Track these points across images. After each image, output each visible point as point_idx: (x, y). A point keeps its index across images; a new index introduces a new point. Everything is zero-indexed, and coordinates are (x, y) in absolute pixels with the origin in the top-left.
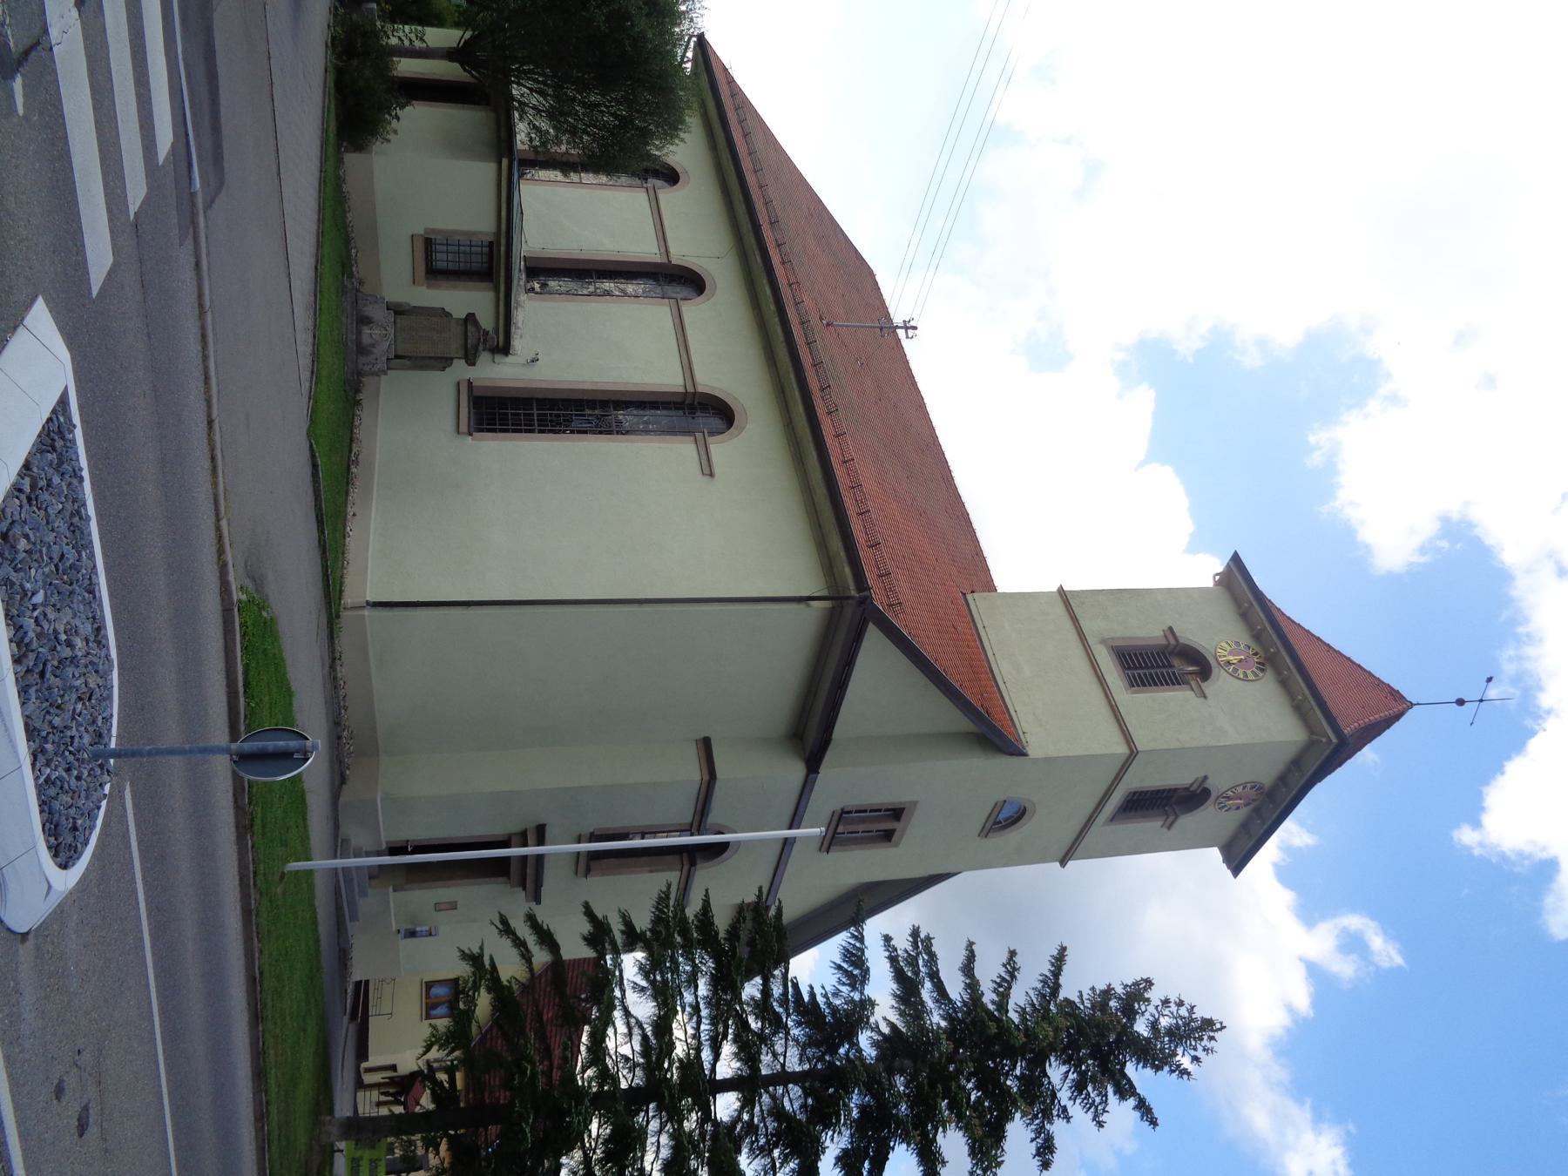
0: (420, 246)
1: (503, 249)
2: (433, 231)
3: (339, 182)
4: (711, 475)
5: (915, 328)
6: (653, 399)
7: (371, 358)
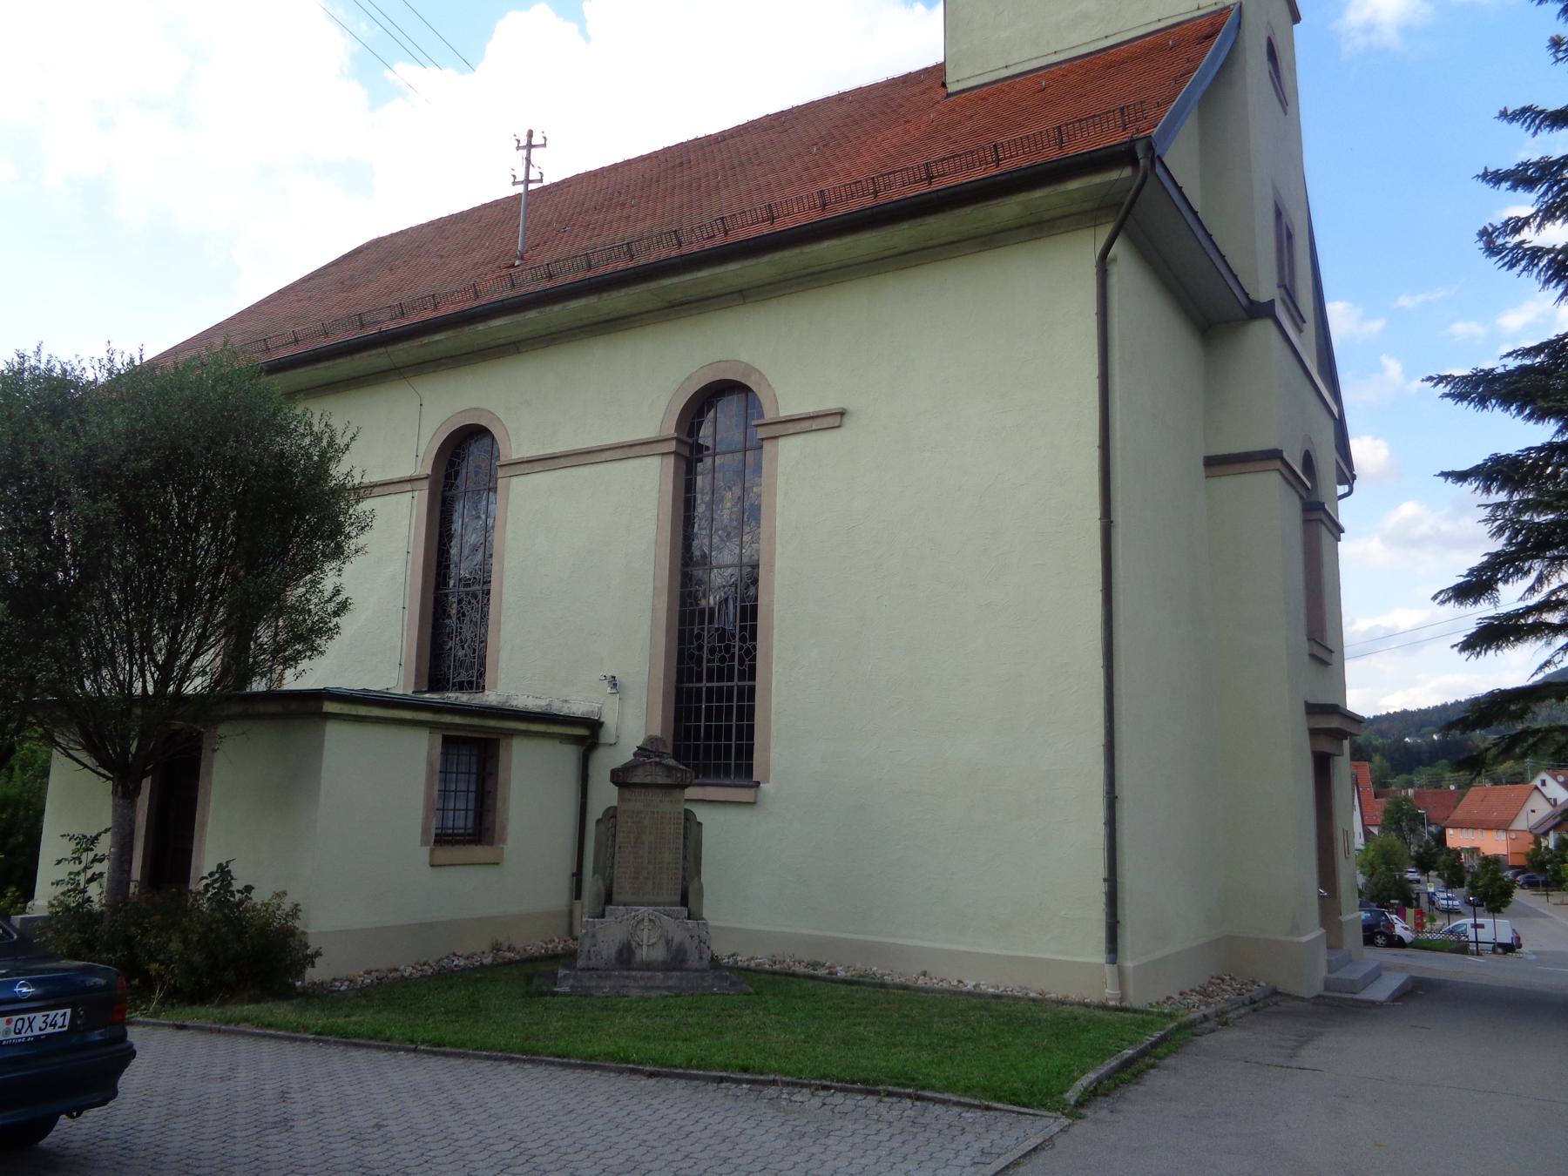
0: (445, 853)
1: (458, 720)
2: (425, 831)
3: (386, 991)
4: (842, 413)
5: (530, 134)
6: (682, 506)
7: (691, 946)
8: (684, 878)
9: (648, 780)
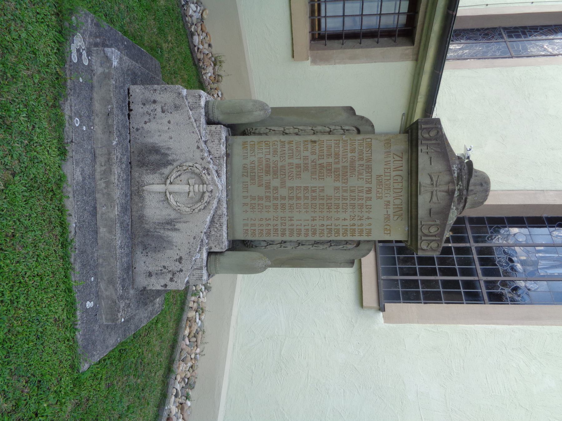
8: (270, 243)
9: (423, 179)
